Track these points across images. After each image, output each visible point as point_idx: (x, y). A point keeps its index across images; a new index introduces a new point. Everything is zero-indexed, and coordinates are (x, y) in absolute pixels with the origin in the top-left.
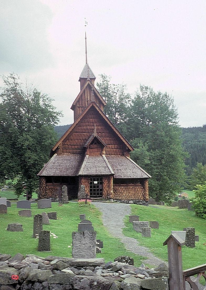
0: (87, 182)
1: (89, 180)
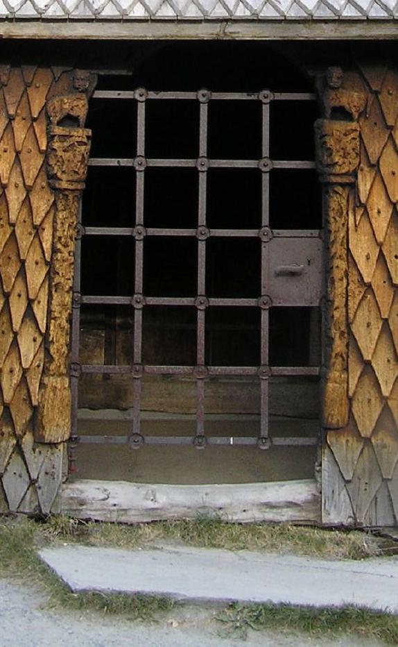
0: (33, 164)
1: (69, 120)
